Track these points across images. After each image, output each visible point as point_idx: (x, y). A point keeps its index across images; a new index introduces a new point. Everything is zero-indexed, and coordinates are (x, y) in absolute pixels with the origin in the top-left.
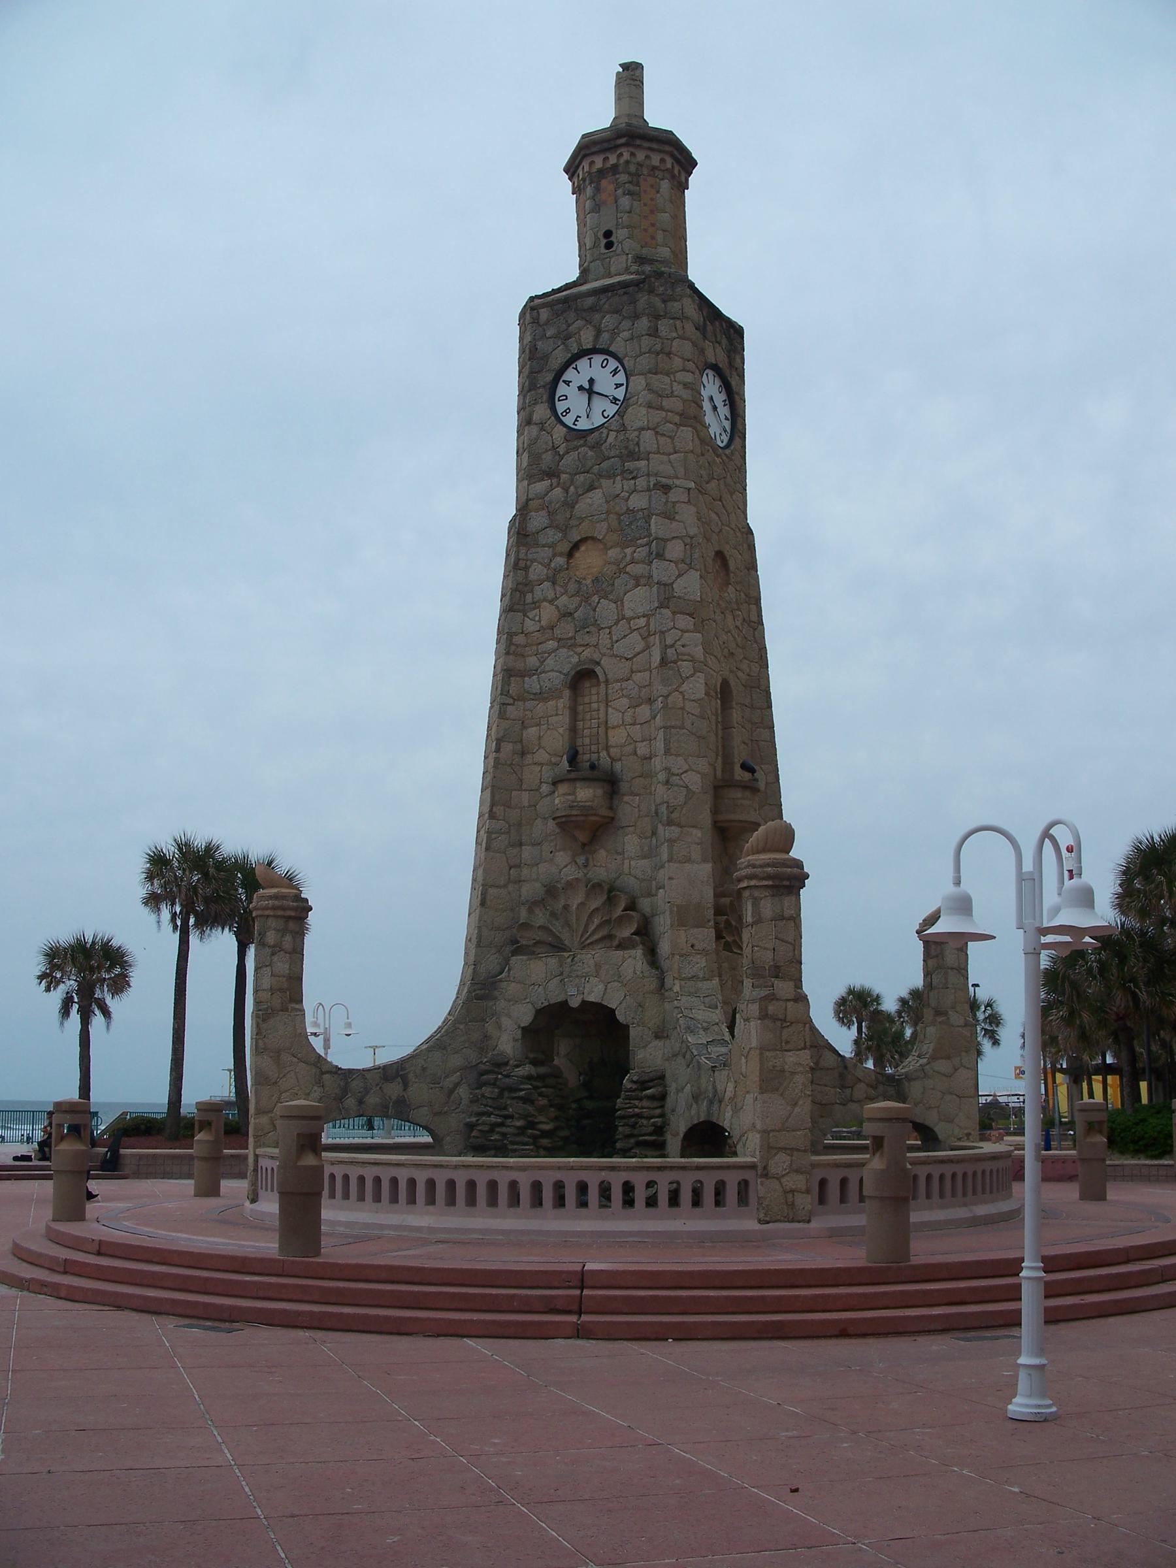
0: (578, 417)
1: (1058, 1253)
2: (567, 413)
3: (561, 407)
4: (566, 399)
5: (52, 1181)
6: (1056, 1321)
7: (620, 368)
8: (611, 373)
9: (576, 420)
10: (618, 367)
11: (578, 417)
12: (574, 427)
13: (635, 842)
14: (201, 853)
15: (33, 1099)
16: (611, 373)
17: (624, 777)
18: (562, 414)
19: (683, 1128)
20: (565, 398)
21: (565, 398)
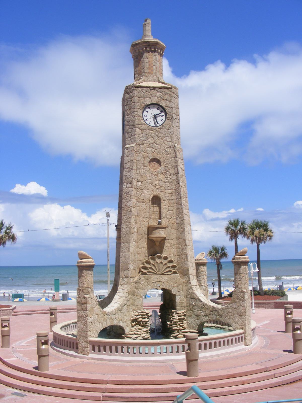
0: (150, 122)
1: (208, 376)
2: (147, 120)
3: (145, 113)
4: (147, 116)
5: (118, 347)
6: (197, 359)
7: (164, 121)
8: (161, 119)
9: (150, 123)
10: (163, 120)
11: (150, 122)
12: (149, 124)
13: (134, 275)
14: (168, 323)
15: (285, 328)
16: (161, 119)
17: (175, 195)
18: (146, 120)
19: (167, 260)
20: (146, 116)
21: (146, 116)
